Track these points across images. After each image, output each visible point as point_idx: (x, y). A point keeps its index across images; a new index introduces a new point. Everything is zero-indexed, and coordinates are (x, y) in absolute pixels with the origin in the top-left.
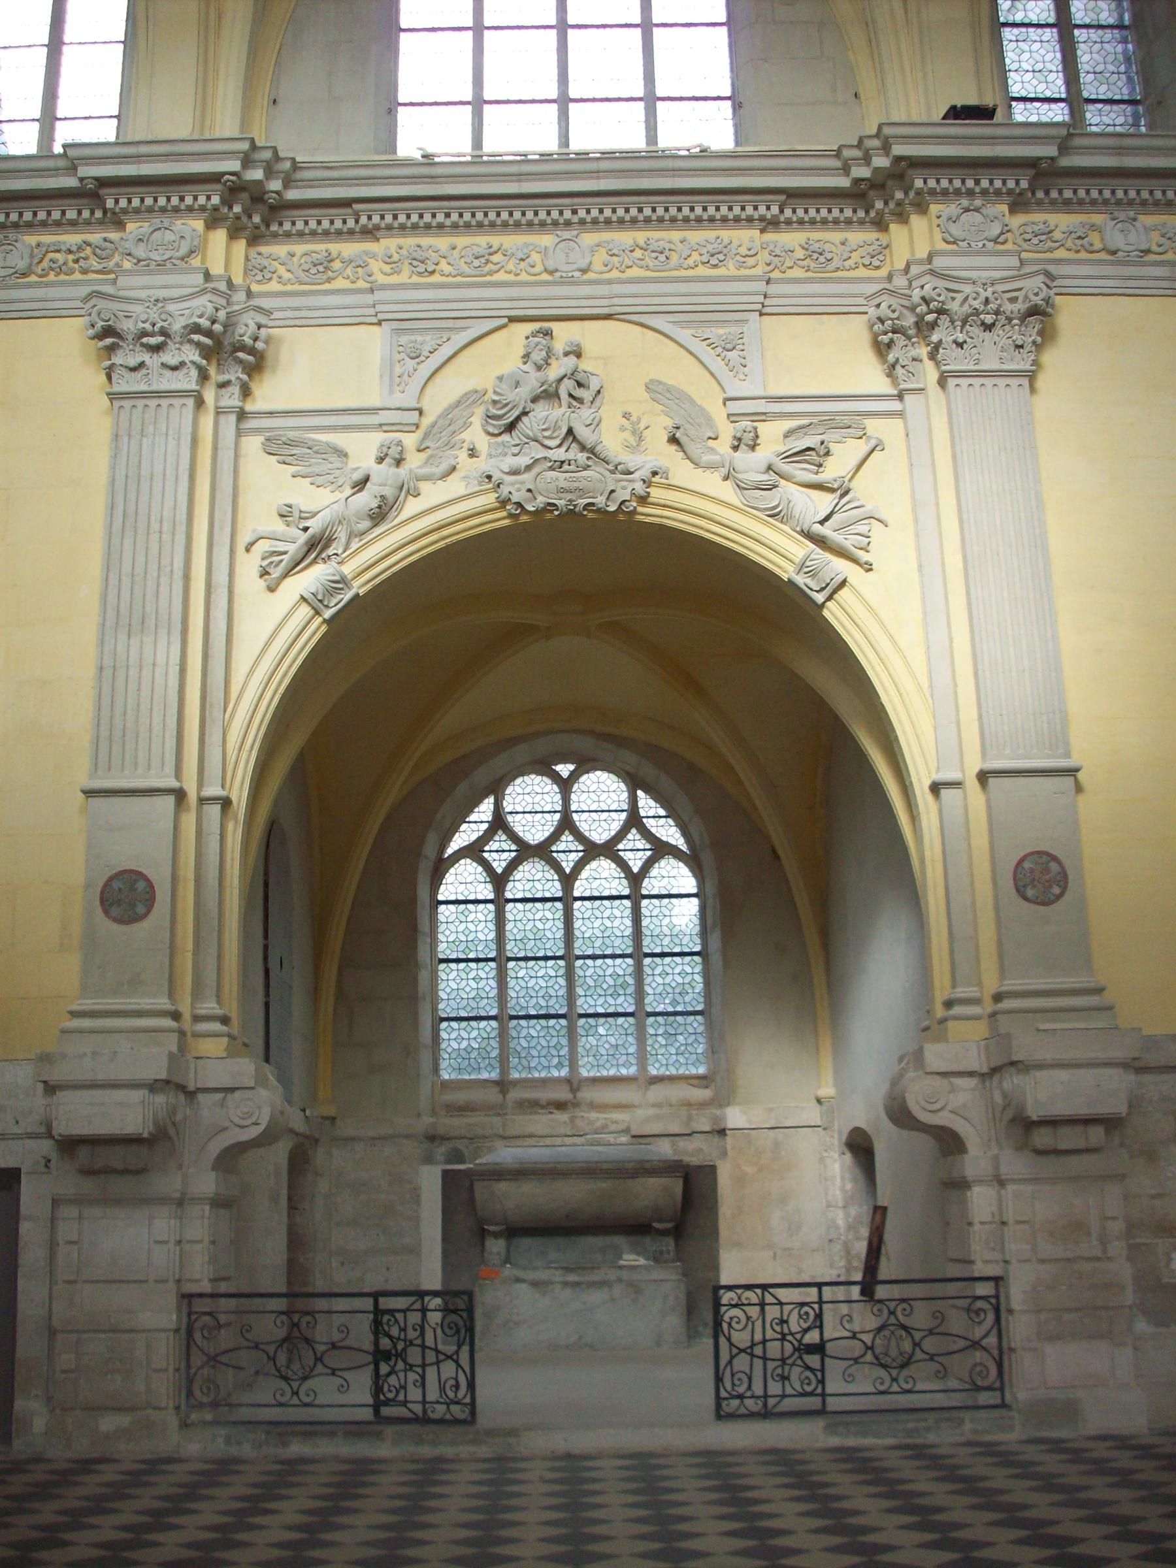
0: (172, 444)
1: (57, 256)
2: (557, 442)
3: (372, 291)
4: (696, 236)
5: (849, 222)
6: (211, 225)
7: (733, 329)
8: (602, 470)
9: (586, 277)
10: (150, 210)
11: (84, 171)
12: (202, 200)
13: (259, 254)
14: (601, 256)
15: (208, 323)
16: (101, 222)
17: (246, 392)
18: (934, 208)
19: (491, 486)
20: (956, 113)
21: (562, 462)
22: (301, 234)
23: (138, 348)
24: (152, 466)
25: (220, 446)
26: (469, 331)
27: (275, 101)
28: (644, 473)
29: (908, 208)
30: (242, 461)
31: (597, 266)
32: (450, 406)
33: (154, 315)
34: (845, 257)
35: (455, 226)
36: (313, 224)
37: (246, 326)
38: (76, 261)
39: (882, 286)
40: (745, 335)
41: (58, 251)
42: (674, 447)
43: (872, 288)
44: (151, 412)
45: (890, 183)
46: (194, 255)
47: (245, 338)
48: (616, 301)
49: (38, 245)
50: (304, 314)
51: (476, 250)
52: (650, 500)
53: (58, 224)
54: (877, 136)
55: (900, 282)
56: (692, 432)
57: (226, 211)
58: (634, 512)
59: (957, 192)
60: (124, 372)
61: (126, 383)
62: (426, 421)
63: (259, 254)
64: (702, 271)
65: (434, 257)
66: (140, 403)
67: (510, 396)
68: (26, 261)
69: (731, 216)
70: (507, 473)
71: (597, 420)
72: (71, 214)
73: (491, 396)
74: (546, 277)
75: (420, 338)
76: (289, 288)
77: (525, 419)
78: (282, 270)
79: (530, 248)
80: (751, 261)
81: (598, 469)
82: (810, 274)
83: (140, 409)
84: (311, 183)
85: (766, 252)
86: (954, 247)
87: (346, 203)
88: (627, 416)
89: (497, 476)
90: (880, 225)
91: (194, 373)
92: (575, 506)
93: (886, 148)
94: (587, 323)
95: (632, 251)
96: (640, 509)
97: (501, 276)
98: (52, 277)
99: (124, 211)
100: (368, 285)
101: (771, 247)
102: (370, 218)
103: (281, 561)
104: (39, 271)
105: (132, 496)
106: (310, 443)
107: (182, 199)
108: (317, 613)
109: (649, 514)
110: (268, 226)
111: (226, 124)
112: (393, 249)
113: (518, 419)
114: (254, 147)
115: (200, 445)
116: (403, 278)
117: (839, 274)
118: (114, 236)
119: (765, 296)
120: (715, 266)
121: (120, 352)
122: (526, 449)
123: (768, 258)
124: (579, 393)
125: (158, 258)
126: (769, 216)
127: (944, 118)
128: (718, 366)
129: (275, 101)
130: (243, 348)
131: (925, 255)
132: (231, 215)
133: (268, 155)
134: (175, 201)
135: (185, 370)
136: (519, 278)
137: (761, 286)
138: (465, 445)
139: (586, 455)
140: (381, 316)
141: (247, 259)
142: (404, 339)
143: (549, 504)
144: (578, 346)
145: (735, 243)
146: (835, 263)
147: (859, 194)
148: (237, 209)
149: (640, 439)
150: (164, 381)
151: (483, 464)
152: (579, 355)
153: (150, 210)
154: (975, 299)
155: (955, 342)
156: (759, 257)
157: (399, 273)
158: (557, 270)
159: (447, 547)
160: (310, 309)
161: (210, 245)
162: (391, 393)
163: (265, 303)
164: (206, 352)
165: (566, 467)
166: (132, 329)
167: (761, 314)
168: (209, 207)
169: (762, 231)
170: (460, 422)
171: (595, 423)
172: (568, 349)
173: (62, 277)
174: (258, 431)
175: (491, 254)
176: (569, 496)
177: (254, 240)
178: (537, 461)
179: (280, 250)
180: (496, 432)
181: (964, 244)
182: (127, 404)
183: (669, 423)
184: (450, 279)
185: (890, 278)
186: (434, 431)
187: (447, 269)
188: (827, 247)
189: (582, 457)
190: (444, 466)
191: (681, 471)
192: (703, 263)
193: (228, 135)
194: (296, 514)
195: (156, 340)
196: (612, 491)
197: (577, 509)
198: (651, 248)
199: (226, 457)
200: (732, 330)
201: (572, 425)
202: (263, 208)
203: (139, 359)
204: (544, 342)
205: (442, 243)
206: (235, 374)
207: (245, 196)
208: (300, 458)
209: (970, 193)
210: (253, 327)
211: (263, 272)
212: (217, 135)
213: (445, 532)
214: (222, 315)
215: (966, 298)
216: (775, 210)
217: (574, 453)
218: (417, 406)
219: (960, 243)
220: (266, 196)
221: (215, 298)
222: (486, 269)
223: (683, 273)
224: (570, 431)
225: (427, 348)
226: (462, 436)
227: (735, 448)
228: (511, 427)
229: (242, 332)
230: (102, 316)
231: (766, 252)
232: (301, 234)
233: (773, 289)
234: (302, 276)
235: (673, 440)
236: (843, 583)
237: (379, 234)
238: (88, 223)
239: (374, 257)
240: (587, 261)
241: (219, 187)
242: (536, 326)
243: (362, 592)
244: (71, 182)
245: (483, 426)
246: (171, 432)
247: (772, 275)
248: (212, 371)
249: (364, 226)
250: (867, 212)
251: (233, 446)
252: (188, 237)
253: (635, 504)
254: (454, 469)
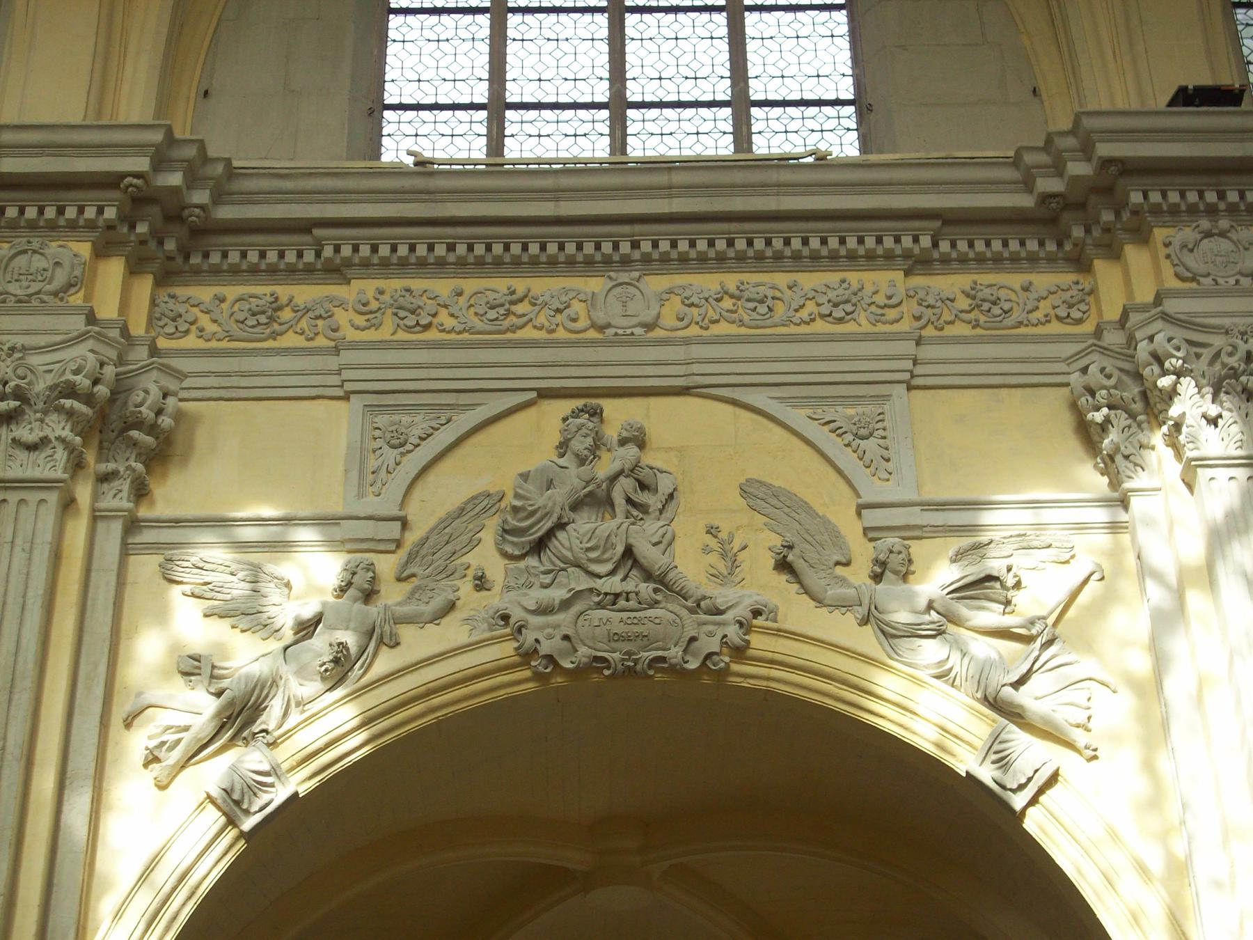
0: (19, 557)
2: (609, 567)
3: (337, 351)
4: (810, 280)
5: (1033, 259)
6: (102, 251)
7: (870, 409)
8: (677, 609)
9: (651, 335)
13: (173, 297)
14: (675, 305)
17: (141, 492)
18: (1159, 234)
19: (508, 630)
20: (1186, 97)
21: (617, 596)
26: (479, 408)
27: (206, 93)
28: (742, 611)
29: (1122, 236)
30: (128, 591)
31: (669, 320)
32: (449, 515)
34: (1029, 307)
35: (461, 263)
37: (147, 392)
39: (1091, 341)
40: (887, 417)
42: (784, 577)
43: (1070, 349)
45: (1093, 199)
46: (73, 290)
47: (143, 409)
48: (696, 368)
50: (234, 381)
51: (491, 296)
52: (751, 652)
54: (1072, 132)
55: (1113, 338)
56: (811, 555)
57: (125, 230)
58: (725, 672)
59: (1193, 210)
62: (412, 538)
63: (173, 297)
64: (820, 326)
65: (430, 306)
67: (541, 500)
69: (861, 251)
70: (533, 612)
71: (668, 536)
73: (510, 500)
74: (592, 334)
75: (406, 419)
76: (214, 344)
77: (561, 535)
78: (204, 321)
79: (571, 295)
80: (892, 314)
81: (669, 606)
82: (979, 331)
84: (251, 198)
85: (914, 302)
86: (1194, 285)
87: (305, 227)
88: (712, 531)
89: (517, 615)
90: (1081, 264)
91: (61, 455)
92: (636, 662)
93: (1086, 151)
94: (653, 401)
95: (718, 300)
96: (735, 667)
97: (528, 333)
100: (333, 344)
101: (921, 294)
102: (337, 249)
103: (178, 741)
107: (61, 211)
108: (231, 822)
109: (747, 674)
110: (187, 257)
111: (135, 102)
112: (370, 294)
113: (550, 533)
114: (170, 140)
116: (385, 333)
117: (1023, 330)
119: (915, 363)
120: (840, 320)
122: (562, 578)
123: (917, 310)
124: (643, 497)
125: (19, 292)
126: (917, 251)
127: (1171, 104)
128: (847, 460)
129: (206, 93)
130: (139, 424)
131: (1150, 298)
133: (190, 152)
136: (554, 336)
137: (909, 347)
138: (471, 573)
139: (652, 586)
140: (349, 386)
141: (153, 303)
142: (382, 420)
143: (596, 659)
144: (641, 430)
145: (869, 289)
146: (1017, 315)
147: (1049, 218)
148: (142, 228)
149: (734, 564)
151: (494, 600)
152: (642, 445)
154: (1230, 355)
155: (1204, 416)
156: (904, 308)
157: (377, 327)
158: (609, 326)
159: (439, 724)
160: (243, 375)
162: (361, 495)
163: (177, 363)
165: (622, 603)
167: (910, 388)
168: (101, 223)
169: (907, 273)
170: (465, 538)
171: (665, 541)
172: (625, 434)
175: (513, 303)
176: (627, 647)
177: (165, 278)
178: (577, 595)
180: (517, 553)
181: (1208, 281)
183: (777, 541)
184: (453, 336)
185: (1098, 333)
186: (423, 552)
187: (450, 323)
188: (1003, 294)
189: (646, 589)
190: (438, 602)
191: (797, 611)
192: (822, 316)
193: (135, 119)
196: (693, 639)
197: (639, 667)
198: (746, 295)
200: (867, 410)
201: (631, 541)
204: (591, 425)
205: (443, 287)
207: (155, 211)
209: (1212, 211)
210: (155, 391)
211: (179, 324)
212: (121, 120)
213: (436, 701)
214: (109, 371)
215: (1217, 355)
216: (926, 241)
217: (635, 584)
218: (402, 513)
219: (1202, 280)
220: (186, 212)
221: (100, 347)
222: (506, 323)
223: (793, 329)
224: (629, 552)
225: (417, 432)
226: (465, 559)
227: (877, 578)
228: (539, 546)
231: (914, 302)
233: (926, 352)
234: (235, 329)
235: (784, 566)
236: (1053, 779)
237: (349, 273)
239: (342, 305)
240: (653, 312)
241: (116, 194)
242: (579, 403)
243: (303, 790)
245: (496, 544)
246: (19, 541)
247: (924, 333)
248: (90, 457)
249: (328, 260)
250: (1060, 245)
251: (115, 567)
252: (67, 265)
253: (727, 659)
254: (451, 607)
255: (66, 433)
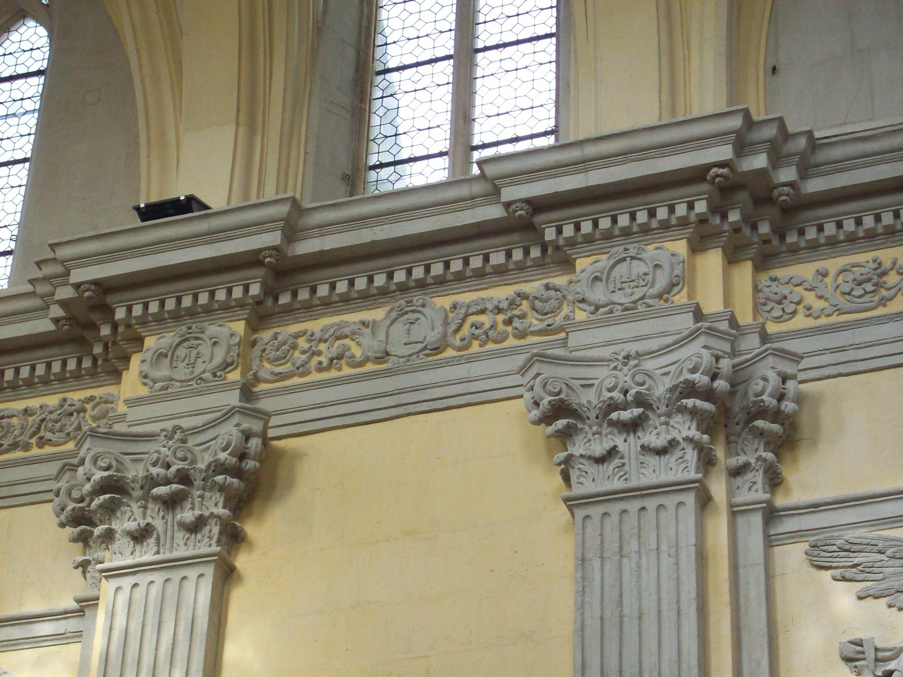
1: (482, 318)
6: (698, 246)
10: (608, 236)
11: (510, 193)
12: (681, 210)
13: (774, 279)
15: (706, 379)
16: (539, 264)
17: (774, 481)
18: (150, 342)
22: (833, 242)
23: (605, 430)
24: (640, 599)
25: (741, 562)
27: (774, 69)
30: (778, 584)
33: (624, 377)
36: (849, 225)
37: (765, 379)
38: (508, 322)
41: (483, 312)
44: (631, 521)
46: (676, 289)
47: (764, 397)
49: (454, 307)
50: (851, 355)
53: (480, 274)
57: (718, 221)
60: (587, 466)
61: (593, 480)
63: (774, 279)
66: (615, 508)
68: (439, 329)
72: (497, 258)
76: (823, 321)
78: (810, 298)
83: (615, 517)
91: (691, 455)
98: (475, 347)
99: (572, 243)
104: (458, 342)
105: (612, 648)
106: (881, 544)
107: (652, 214)
110: (782, 237)
111: (706, 94)
114: (750, 123)
115: (711, 562)
118: (560, 281)
121: (579, 439)
125: (623, 300)
129: (774, 69)
130: (763, 412)
132: (726, 227)
133: (771, 132)
134: (642, 217)
135: (678, 454)
141: (756, 289)
148: (734, 216)
150: (648, 472)
153: (608, 236)
161: (699, 275)
164: (708, 424)
166: (595, 401)
168: (693, 218)
173: (491, 346)
174: (797, 535)
177: (764, 262)
179: (805, 270)
182: (596, 511)
193: (709, 110)
194: (870, 654)
195: (631, 414)
199: (753, 579)
202: (773, 212)
203: (607, 445)
206: (754, 453)
207: (744, 196)
208: (868, 569)
214: (725, 364)
220: (776, 192)
221: (712, 342)
229: (759, 388)
230: (548, 387)
232: (833, 242)
234: (841, 301)
238: (521, 267)
241: (705, 187)
244: (493, 212)
246: (664, 547)
248: (720, 452)
251: (762, 561)
252: (666, 266)
255: (220, 511)
